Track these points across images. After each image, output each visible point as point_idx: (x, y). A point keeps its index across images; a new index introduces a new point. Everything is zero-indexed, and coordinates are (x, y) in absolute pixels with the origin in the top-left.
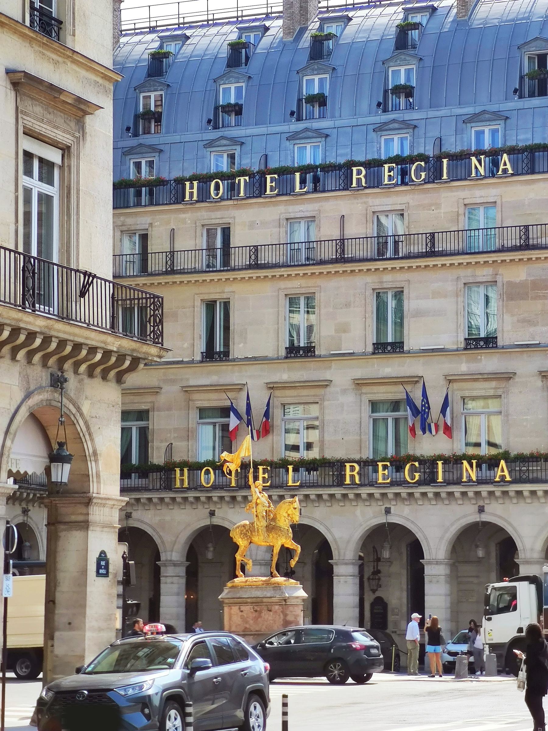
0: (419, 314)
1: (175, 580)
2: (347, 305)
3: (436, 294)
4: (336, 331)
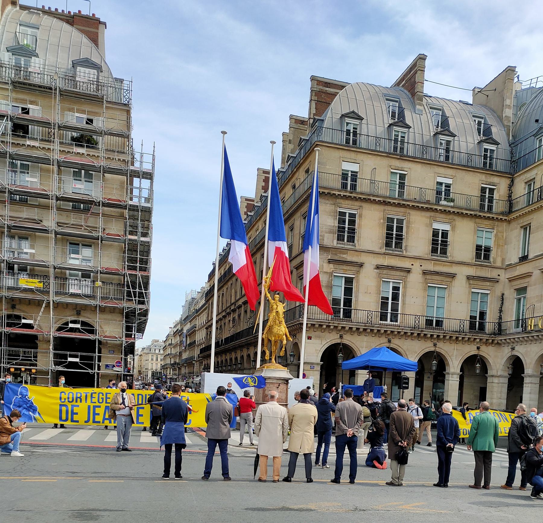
1: (530, 385)
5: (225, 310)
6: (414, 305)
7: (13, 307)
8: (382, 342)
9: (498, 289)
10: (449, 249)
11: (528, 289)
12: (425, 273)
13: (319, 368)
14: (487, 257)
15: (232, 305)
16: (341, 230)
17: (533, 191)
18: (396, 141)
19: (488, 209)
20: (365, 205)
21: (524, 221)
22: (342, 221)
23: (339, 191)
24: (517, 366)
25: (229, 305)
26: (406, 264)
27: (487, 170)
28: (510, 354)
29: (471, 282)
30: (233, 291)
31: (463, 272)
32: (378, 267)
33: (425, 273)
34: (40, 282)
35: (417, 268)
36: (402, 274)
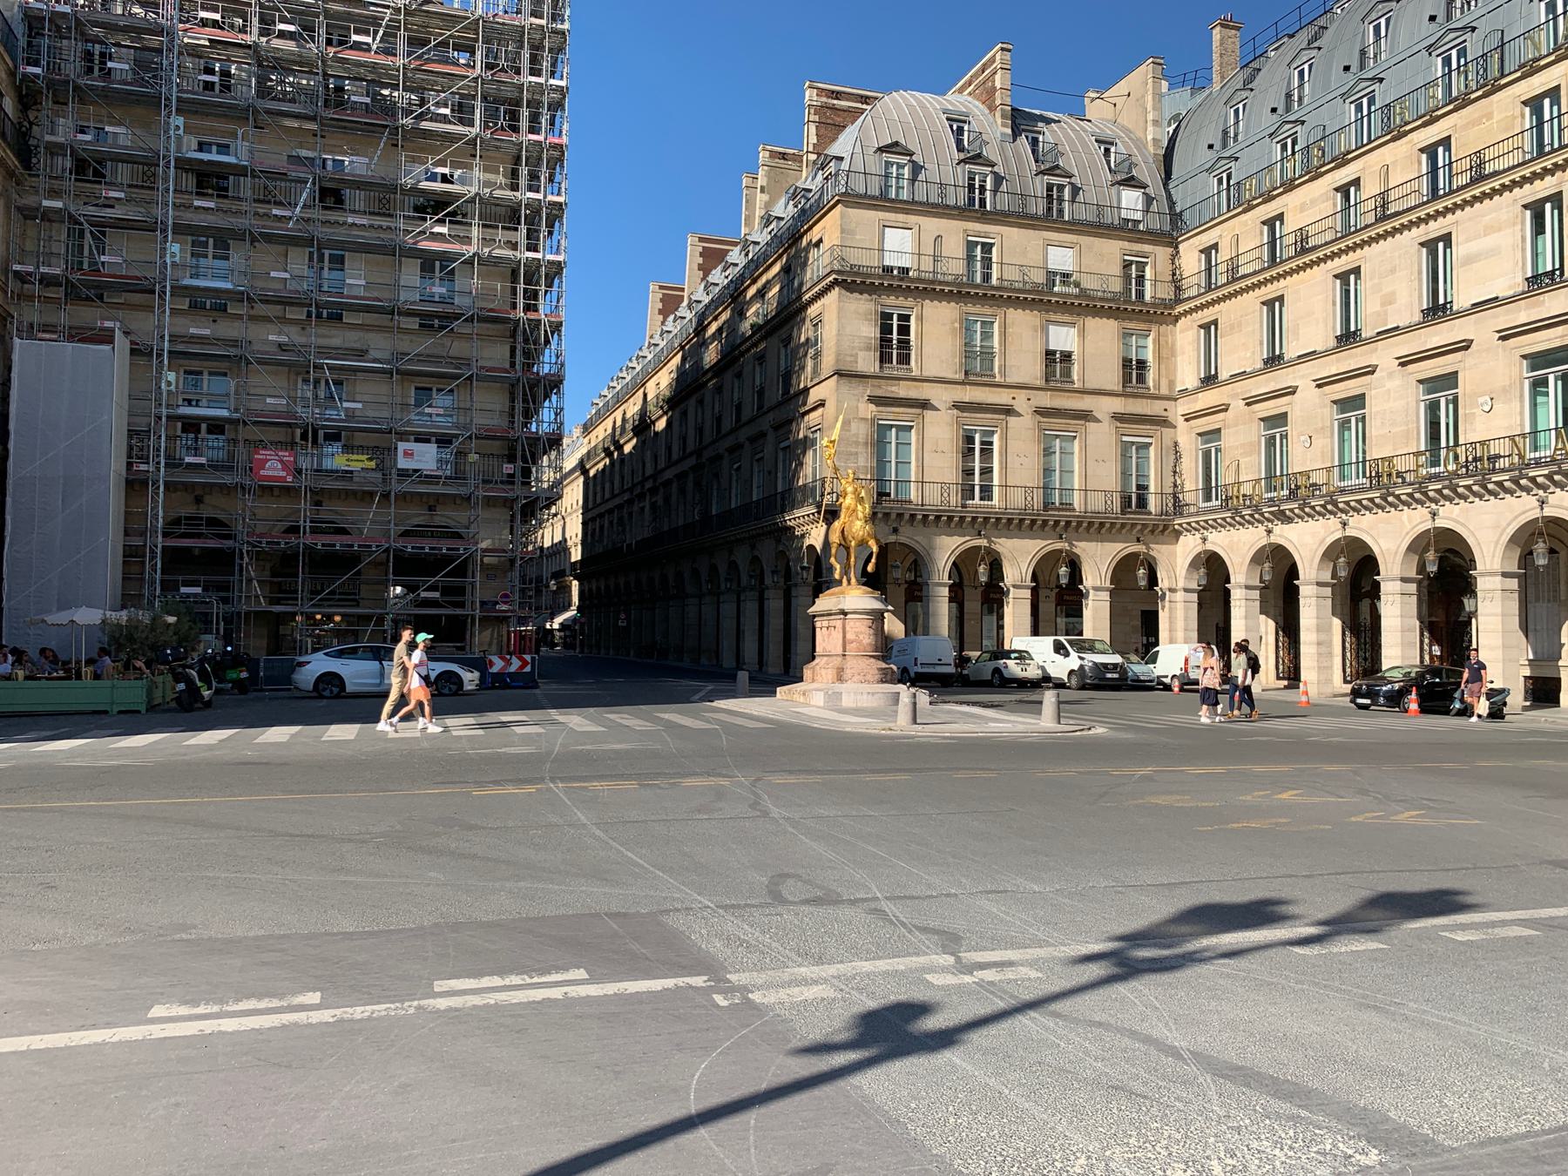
0: (1469, 260)
2: (1393, 271)
3: (1489, 230)
4: (1383, 304)
5: (631, 490)
6: (1015, 473)
7: (319, 503)
14: (1141, 379)
15: (646, 479)
16: (885, 342)
18: (971, 188)
21: (1206, 315)
22: (886, 329)
23: (880, 277)
24: (1213, 568)
27: (1055, 221)
28: (1199, 549)
31: (1105, 407)
34: (370, 459)
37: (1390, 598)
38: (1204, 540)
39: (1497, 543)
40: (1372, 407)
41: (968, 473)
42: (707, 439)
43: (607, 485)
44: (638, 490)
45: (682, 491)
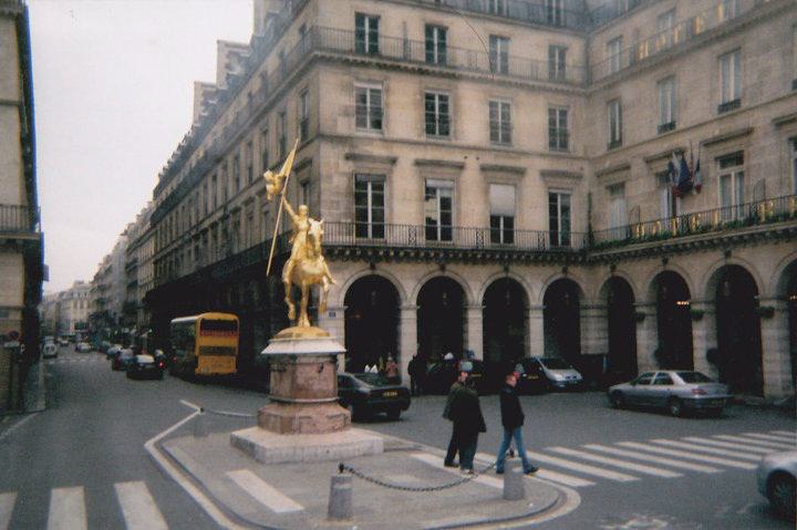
8: (431, 269)
9: (585, 187)
10: (514, 134)
11: (627, 185)
12: (484, 169)
13: (340, 315)
15: (192, 229)
16: (360, 111)
17: (620, 53)
19: (439, 61)
20: (392, 75)
25: (187, 229)
26: (457, 157)
29: (547, 179)
30: (193, 209)
32: (418, 163)
33: (484, 169)
35: (473, 163)
36: (453, 171)
37: (593, 312)
38: (506, 270)
39: (652, 272)
40: (752, 161)
41: (362, 215)
42: (231, 195)
43: (168, 234)
44: (187, 237)
45: (215, 237)
